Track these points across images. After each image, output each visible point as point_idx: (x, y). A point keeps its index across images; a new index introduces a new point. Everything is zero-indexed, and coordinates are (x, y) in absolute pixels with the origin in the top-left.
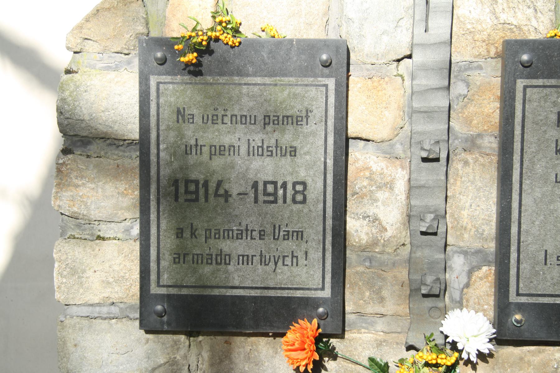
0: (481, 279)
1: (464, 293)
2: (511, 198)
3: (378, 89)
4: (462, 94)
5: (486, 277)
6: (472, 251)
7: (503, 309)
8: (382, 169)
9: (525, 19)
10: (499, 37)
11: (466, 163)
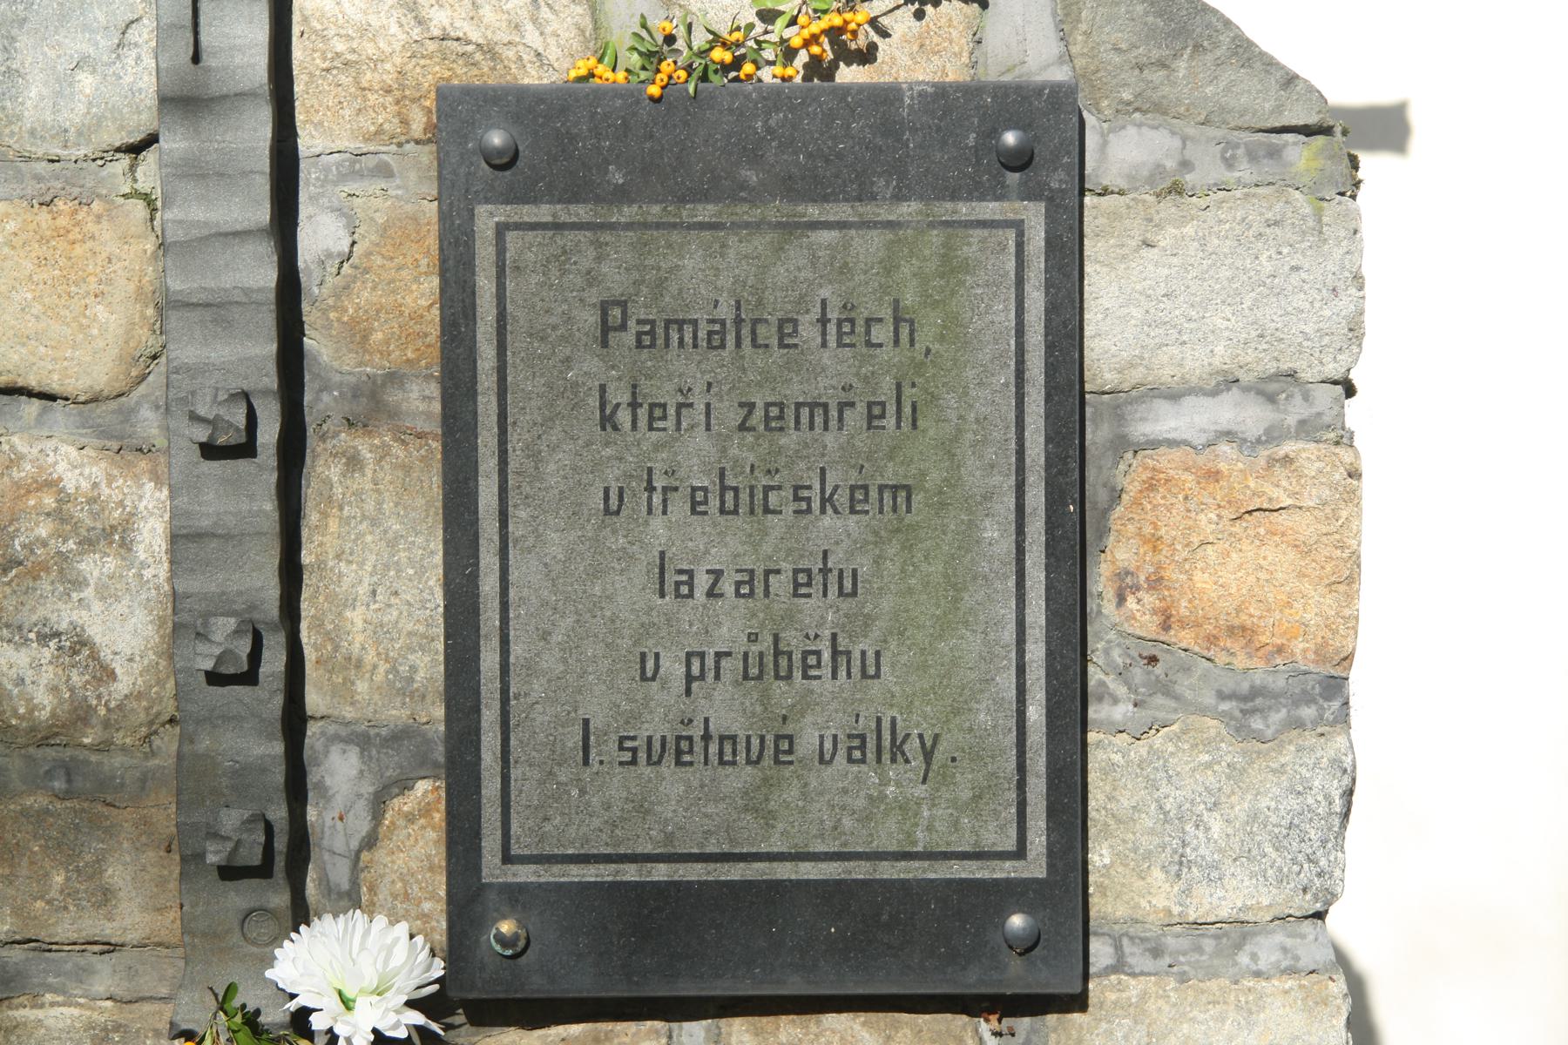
0: (410, 818)
1: (361, 864)
2: (477, 564)
3: (71, 237)
4: (335, 249)
5: (426, 811)
6: (384, 731)
7: (467, 903)
8: (95, 485)
9: (504, 25)
10: (430, 75)
11: (354, 462)
